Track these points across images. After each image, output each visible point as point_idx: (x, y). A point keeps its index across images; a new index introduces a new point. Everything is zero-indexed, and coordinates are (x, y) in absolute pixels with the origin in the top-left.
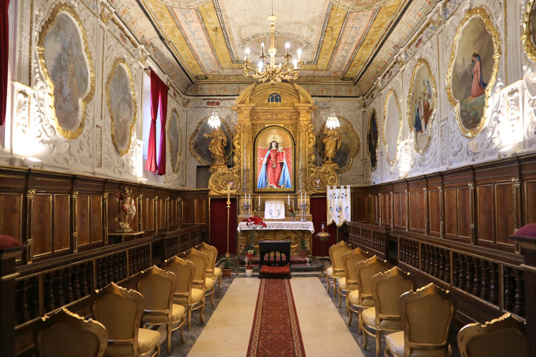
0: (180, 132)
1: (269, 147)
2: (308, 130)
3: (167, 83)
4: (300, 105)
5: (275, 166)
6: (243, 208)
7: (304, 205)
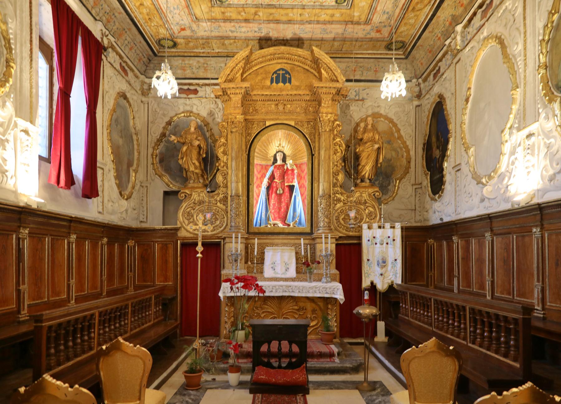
0: (136, 134)
1: (272, 162)
2: (333, 131)
3: (102, 39)
4: (321, 85)
5: (281, 192)
6: (230, 258)
7: (326, 256)
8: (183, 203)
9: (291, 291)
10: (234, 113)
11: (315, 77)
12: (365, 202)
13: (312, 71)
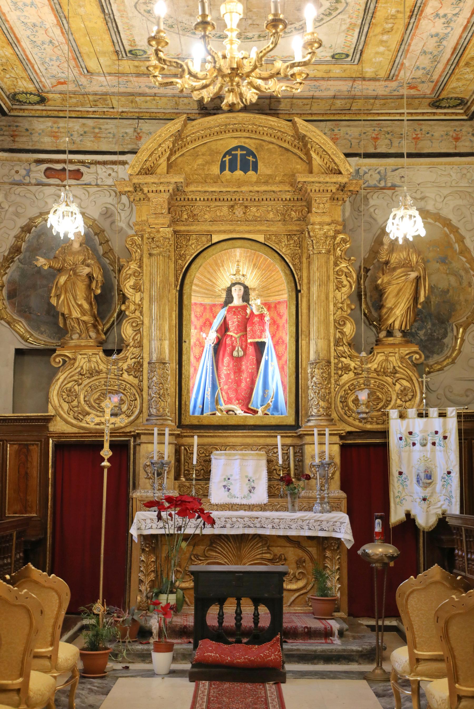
5: (241, 353)
7: (322, 465)
8: (60, 374)
9: (258, 525)
10: (156, 224)
11: (300, 161)
12: (395, 372)
13: (296, 151)
